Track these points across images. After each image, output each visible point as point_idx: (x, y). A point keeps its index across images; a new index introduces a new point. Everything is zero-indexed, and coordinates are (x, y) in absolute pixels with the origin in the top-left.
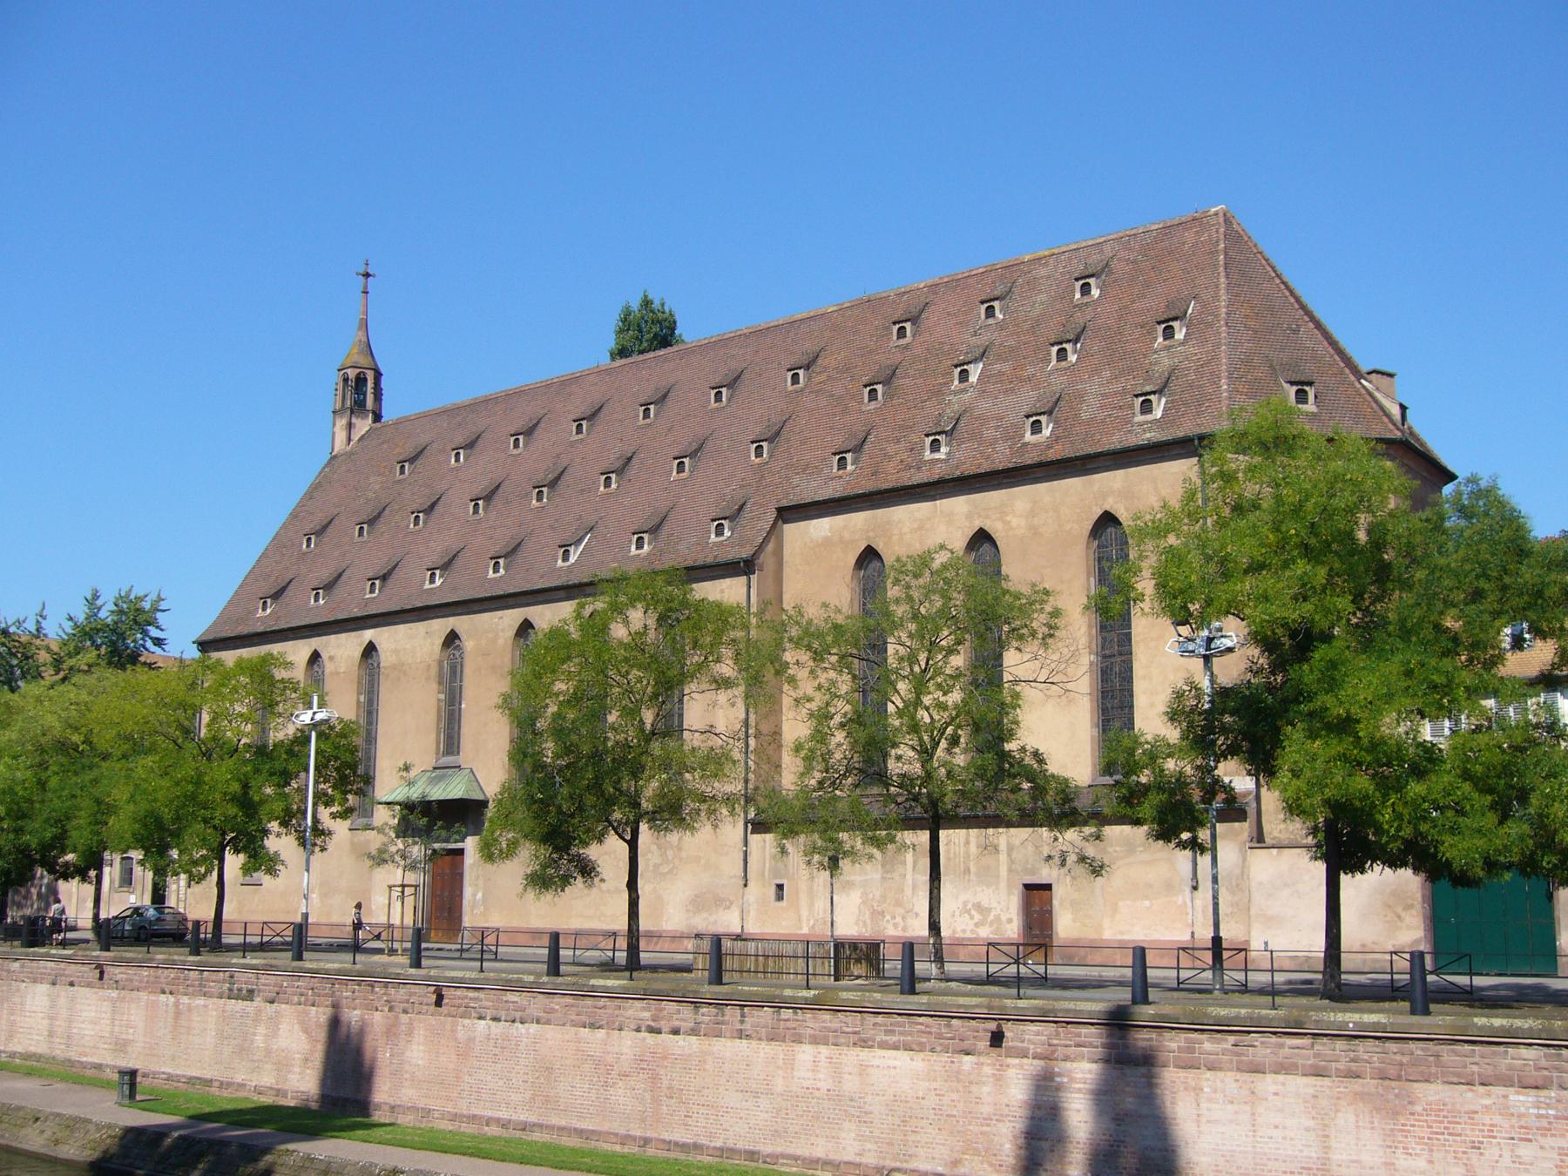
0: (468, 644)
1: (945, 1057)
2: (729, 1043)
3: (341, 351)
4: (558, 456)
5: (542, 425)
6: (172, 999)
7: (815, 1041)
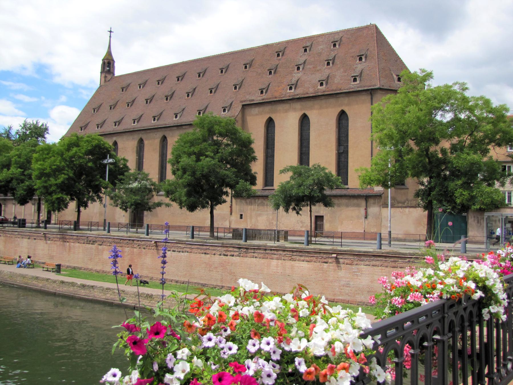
0: (146, 142)
1: (318, 264)
2: (250, 259)
3: (103, 53)
4: (172, 88)
5: (166, 78)
7: (277, 259)
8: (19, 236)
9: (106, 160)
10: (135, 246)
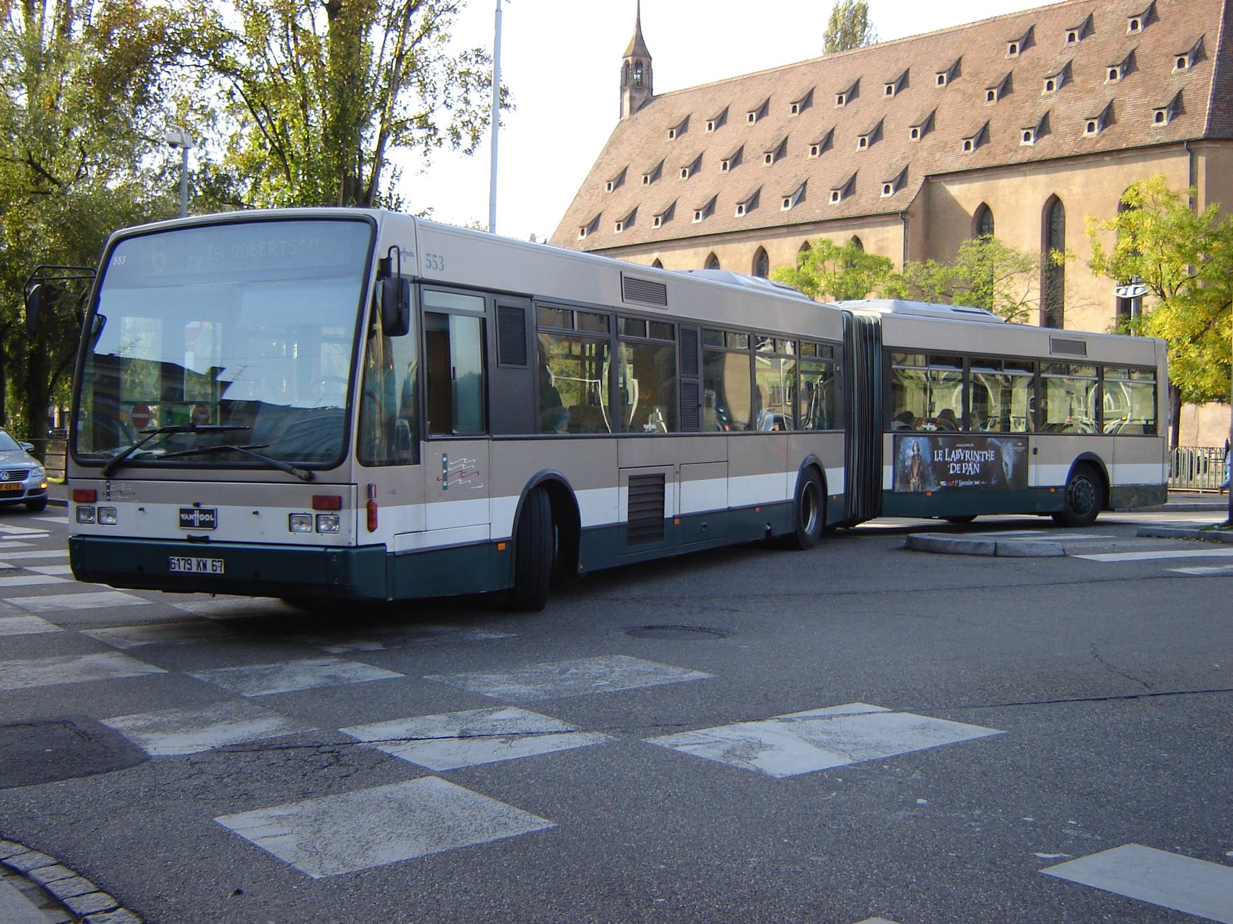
3: (625, 42)
4: (780, 129)
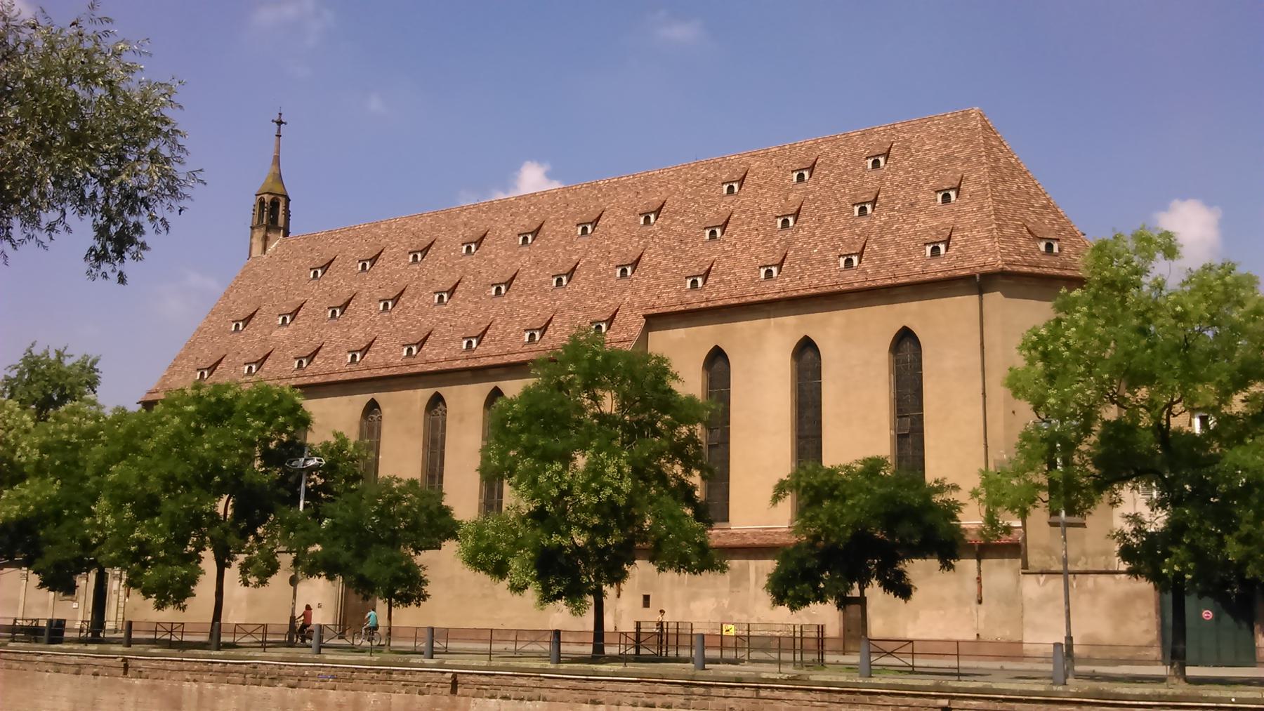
0: (386, 411)
3: (255, 181)
6: (196, 686)
8: (47, 667)
9: (302, 460)
10: (395, 686)
